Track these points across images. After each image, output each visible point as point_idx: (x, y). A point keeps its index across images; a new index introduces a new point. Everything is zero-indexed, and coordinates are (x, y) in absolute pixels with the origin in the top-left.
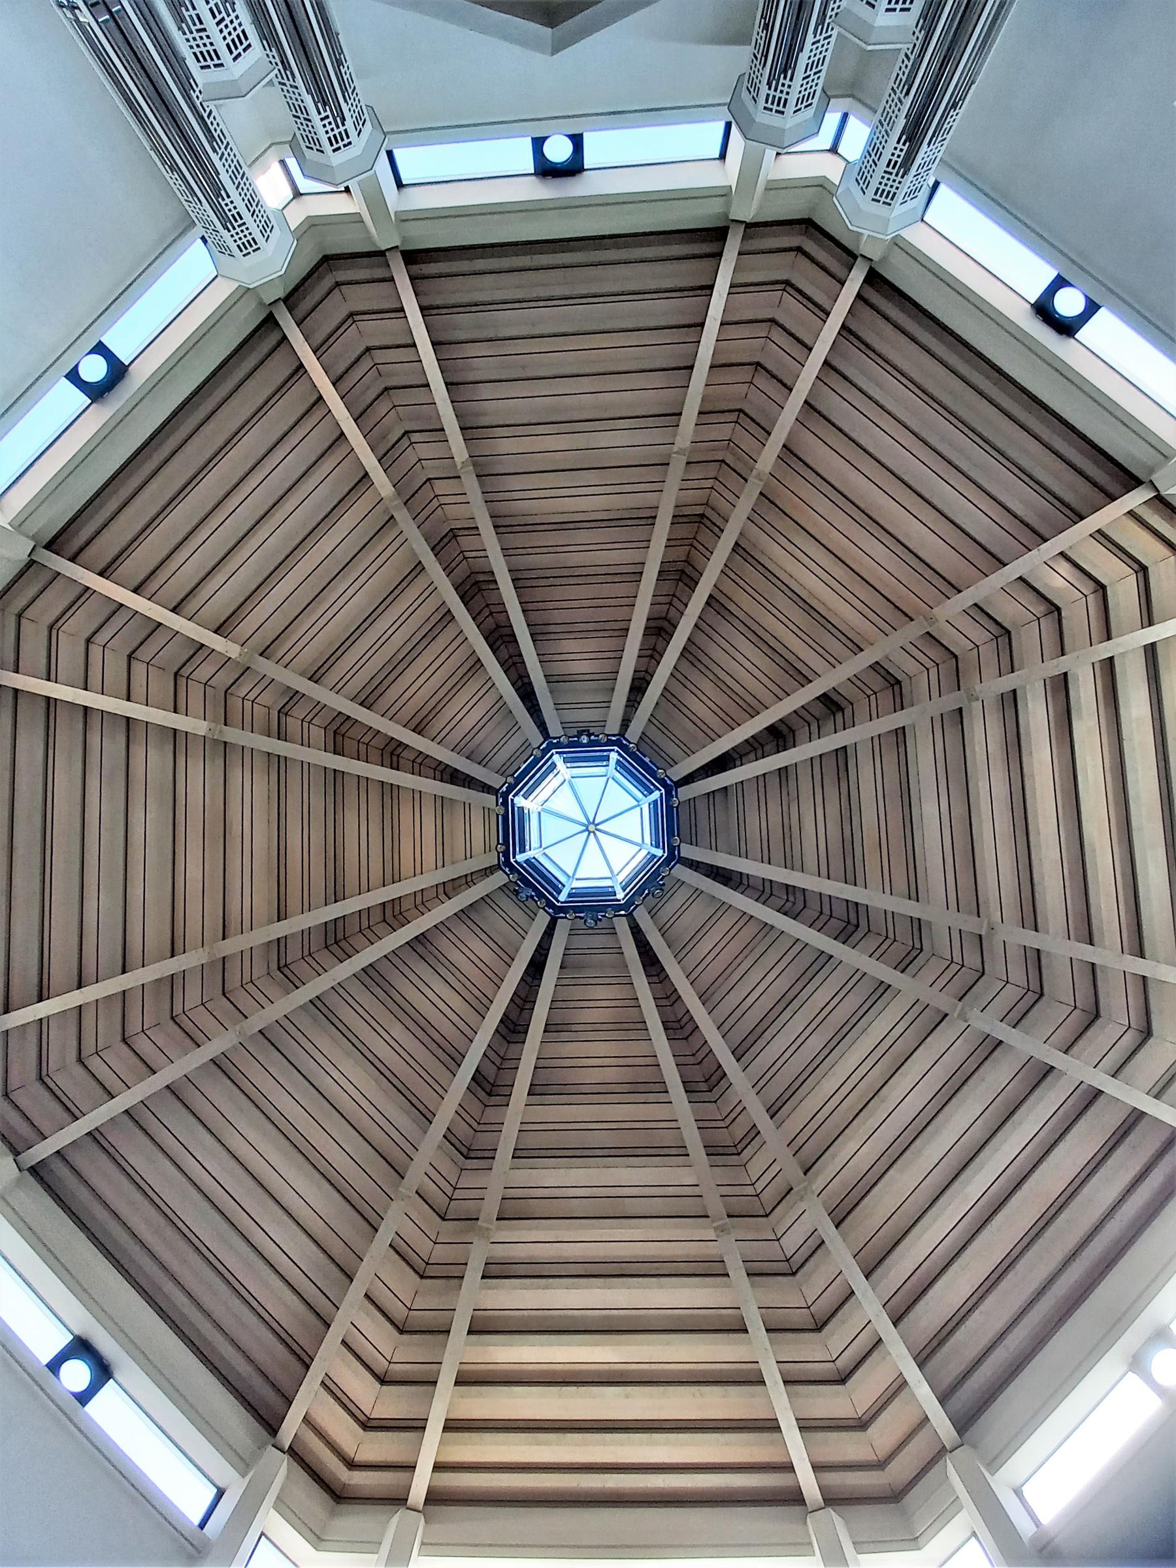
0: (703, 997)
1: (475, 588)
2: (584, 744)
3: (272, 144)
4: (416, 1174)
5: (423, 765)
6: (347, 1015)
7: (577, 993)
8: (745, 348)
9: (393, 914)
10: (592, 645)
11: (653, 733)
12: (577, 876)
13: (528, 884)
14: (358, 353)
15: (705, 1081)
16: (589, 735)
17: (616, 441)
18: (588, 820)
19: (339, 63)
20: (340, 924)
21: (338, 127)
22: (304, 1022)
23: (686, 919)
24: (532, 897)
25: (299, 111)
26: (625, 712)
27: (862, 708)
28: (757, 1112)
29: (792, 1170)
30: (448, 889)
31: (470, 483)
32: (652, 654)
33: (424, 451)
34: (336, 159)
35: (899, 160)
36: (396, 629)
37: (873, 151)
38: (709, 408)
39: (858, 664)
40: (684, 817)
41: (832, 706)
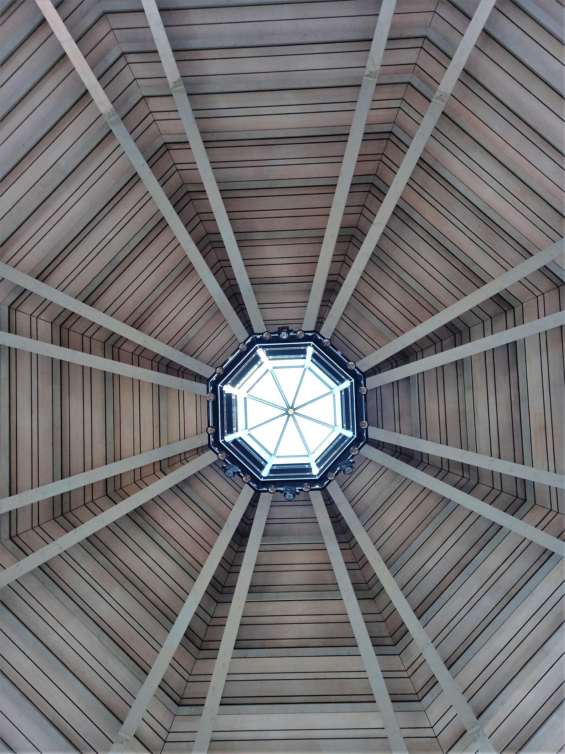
0: (388, 562)
1: (186, 198)
2: (284, 342)
4: (134, 721)
5: (140, 356)
6: (71, 578)
7: (277, 557)
9: (113, 490)
10: (291, 251)
11: (345, 330)
12: (277, 455)
13: (235, 462)
15: (390, 638)
16: (289, 332)
17: (314, 65)
18: (282, 409)
20: (66, 499)
22: (33, 585)
23: (374, 491)
24: (238, 473)
26: (320, 312)
27: (530, 306)
28: (435, 664)
29: (466, 715)
30: (163, 467)
31: (182, 102)
32: (343, 259)
33: (140, 70)
36: (115, 234)
38: (396, 34)
39: (529, 267)
40: (371, 403)
41: (504, 307)
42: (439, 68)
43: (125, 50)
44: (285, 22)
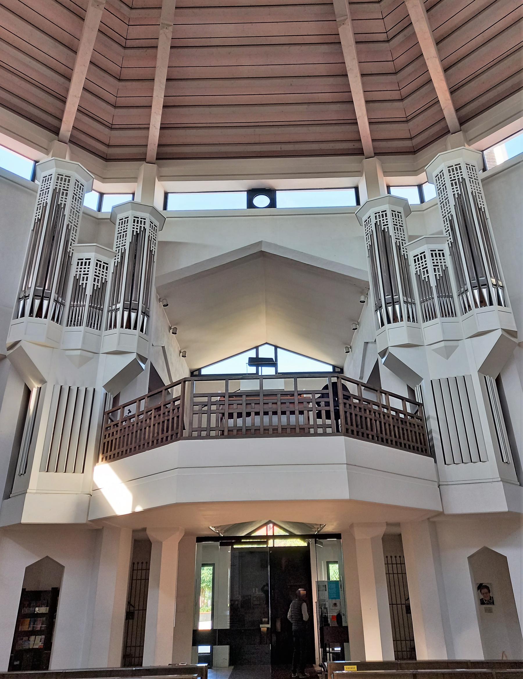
3: (424, 211)
8: (131, 92)
14: (409, 99)
19: (371, 246)
21: (380, 221)
25: (399, 227)
33: (377, 26)
34: (386, 207)
35: (61, 196)
37: (78, 198)
42: (108, 22)
43: (387, 44)
44: (271, 27)
